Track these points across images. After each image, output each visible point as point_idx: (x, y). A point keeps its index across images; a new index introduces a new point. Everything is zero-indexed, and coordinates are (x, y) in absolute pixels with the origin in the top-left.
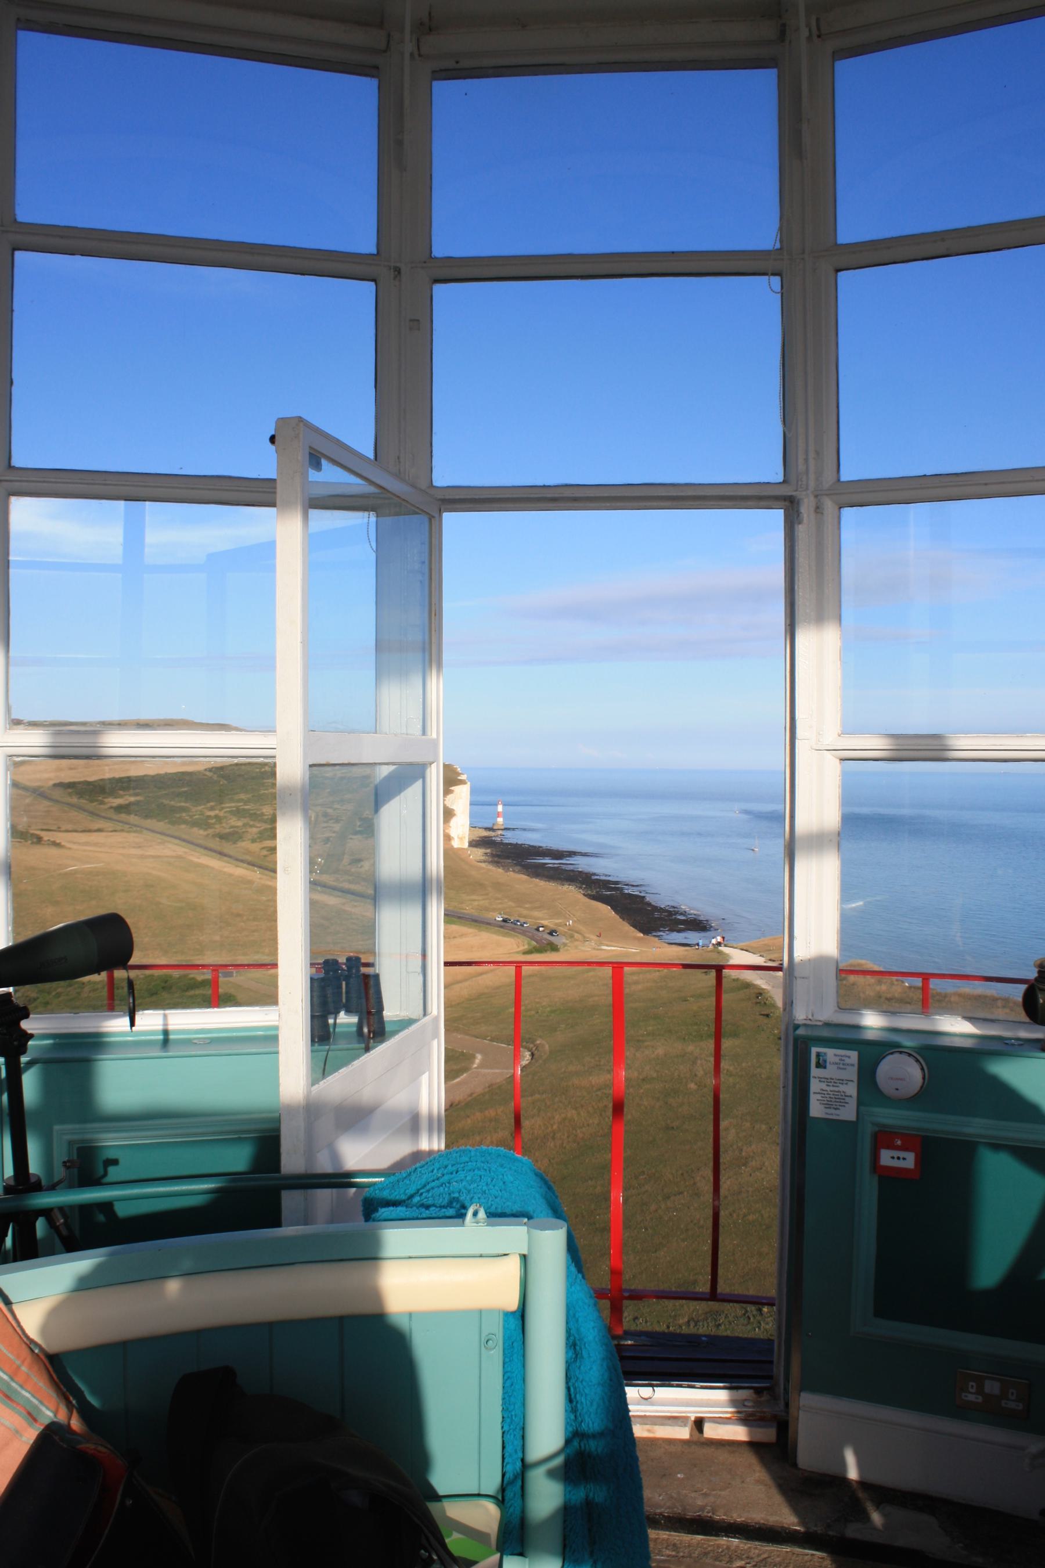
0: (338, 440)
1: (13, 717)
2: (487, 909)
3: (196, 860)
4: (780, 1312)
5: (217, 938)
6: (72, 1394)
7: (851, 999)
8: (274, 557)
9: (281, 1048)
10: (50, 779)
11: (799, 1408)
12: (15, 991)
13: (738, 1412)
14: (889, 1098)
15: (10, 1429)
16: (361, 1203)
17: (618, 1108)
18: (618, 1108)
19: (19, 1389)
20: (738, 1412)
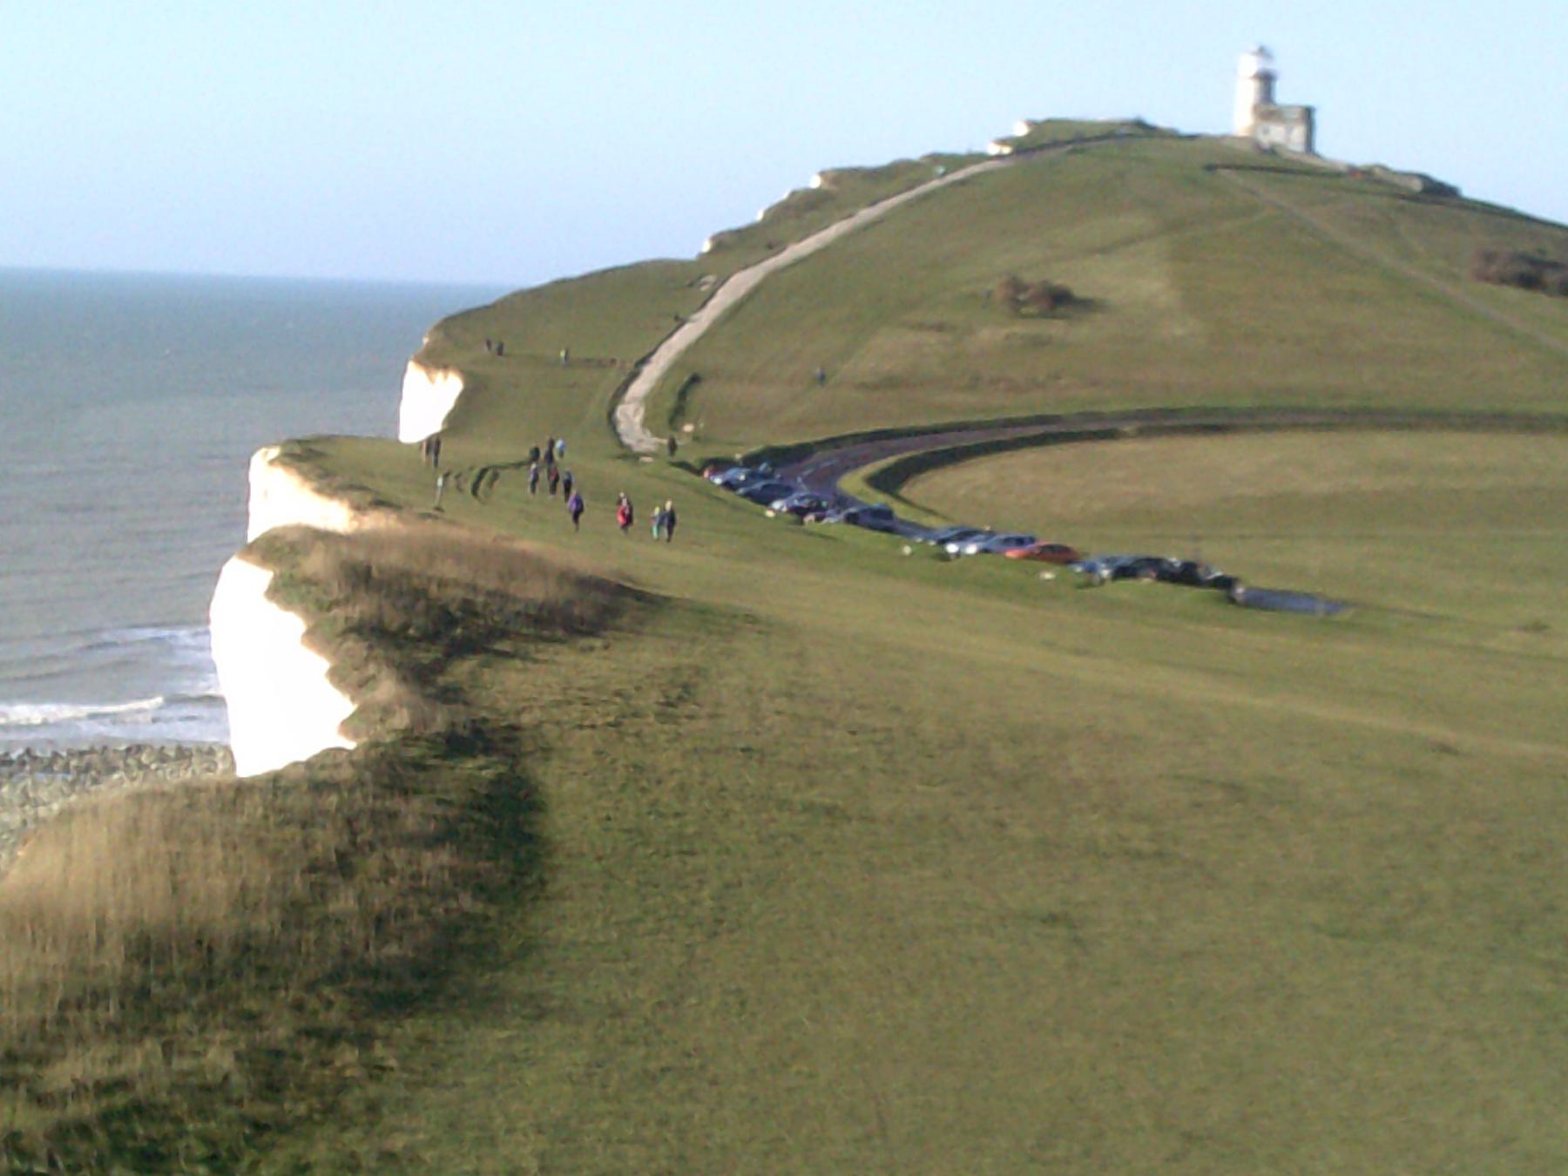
0: (1161, 410)
1: (503, 473)
2: (507, 539)
3: (66, 711)
4: (616, 639)
5: (219, 1057)
6: (897, 465)
7: (431, 558)
8: (216, 583)
9: (212, 628)
10: (540, 568)
11: (504, 597)
12: (695, 423)
13: (101, 923)
14: (618, 435)
15: (179, 922)
16: (273, 608)
17: (629, 519)
18: (629, 519)
19: (772, 263)
20: (101, 923)
